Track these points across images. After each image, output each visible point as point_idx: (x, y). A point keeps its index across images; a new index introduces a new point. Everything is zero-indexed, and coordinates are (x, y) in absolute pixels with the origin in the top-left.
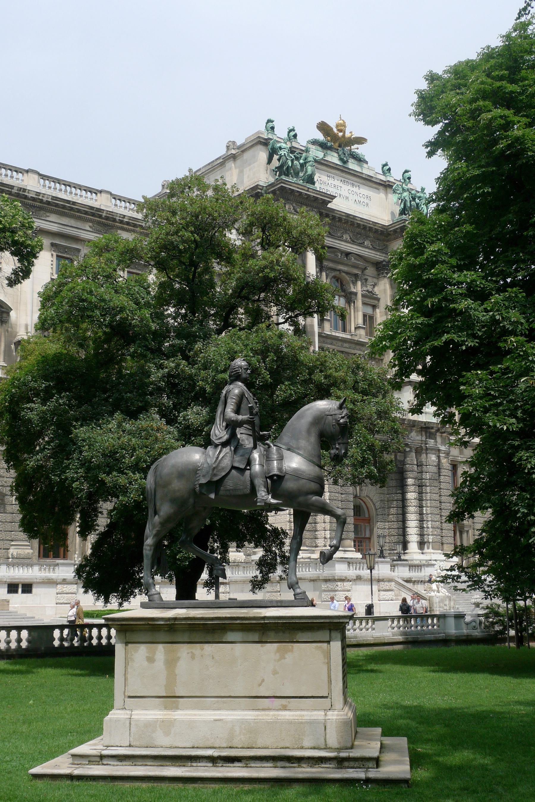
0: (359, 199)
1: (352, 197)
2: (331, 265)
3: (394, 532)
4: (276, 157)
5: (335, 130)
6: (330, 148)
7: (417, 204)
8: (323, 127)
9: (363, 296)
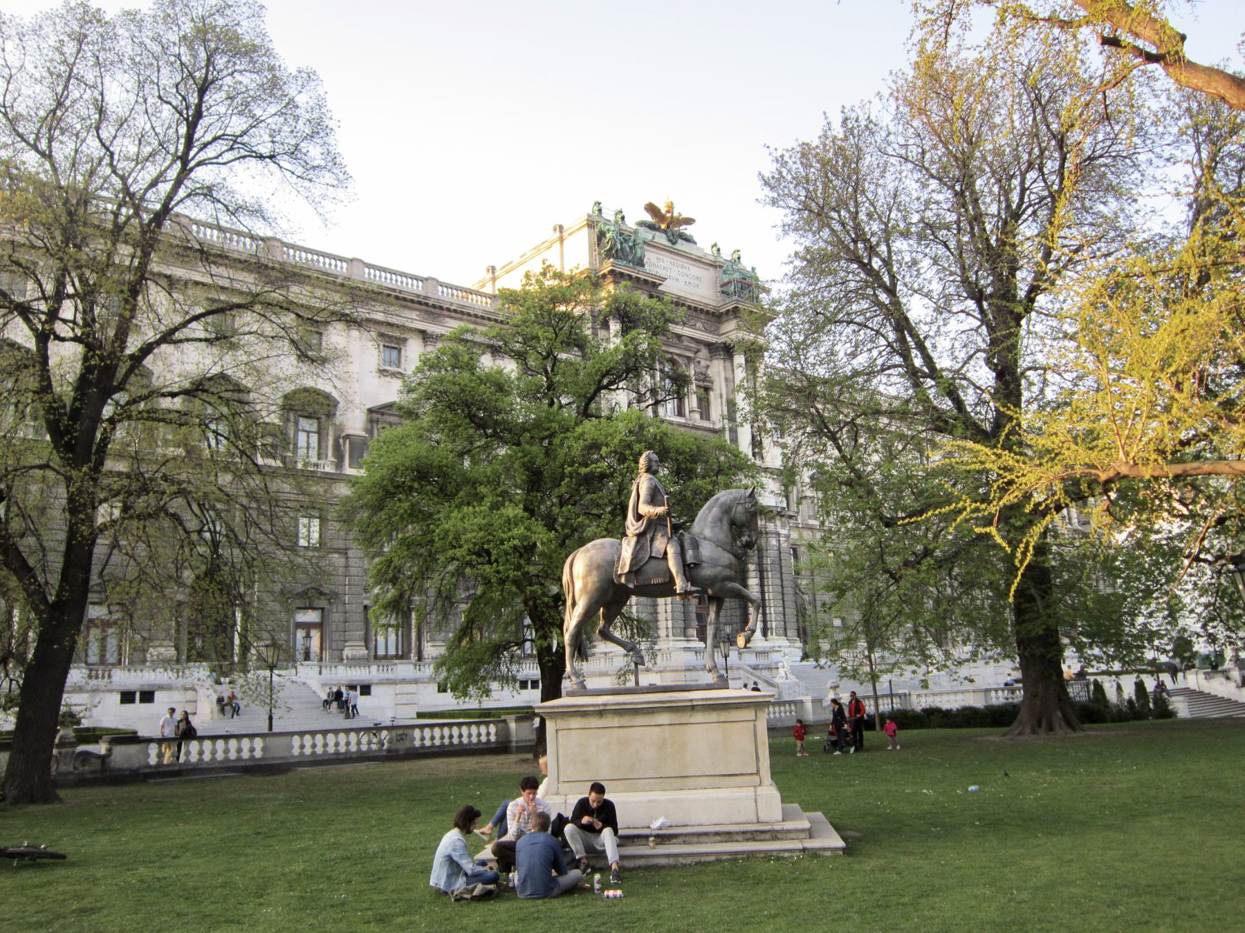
8: (651, 208)
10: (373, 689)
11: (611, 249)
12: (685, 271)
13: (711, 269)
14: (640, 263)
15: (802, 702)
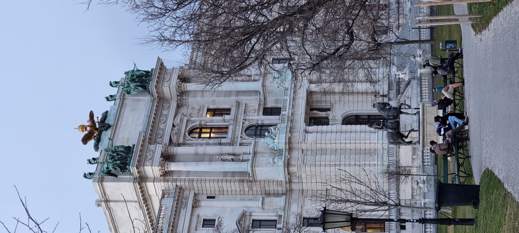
5: (86, 132)
7: (137, 77)
8: (85, 140)
11: (120, 167)
13: (125, 102)
15: (420, 74)
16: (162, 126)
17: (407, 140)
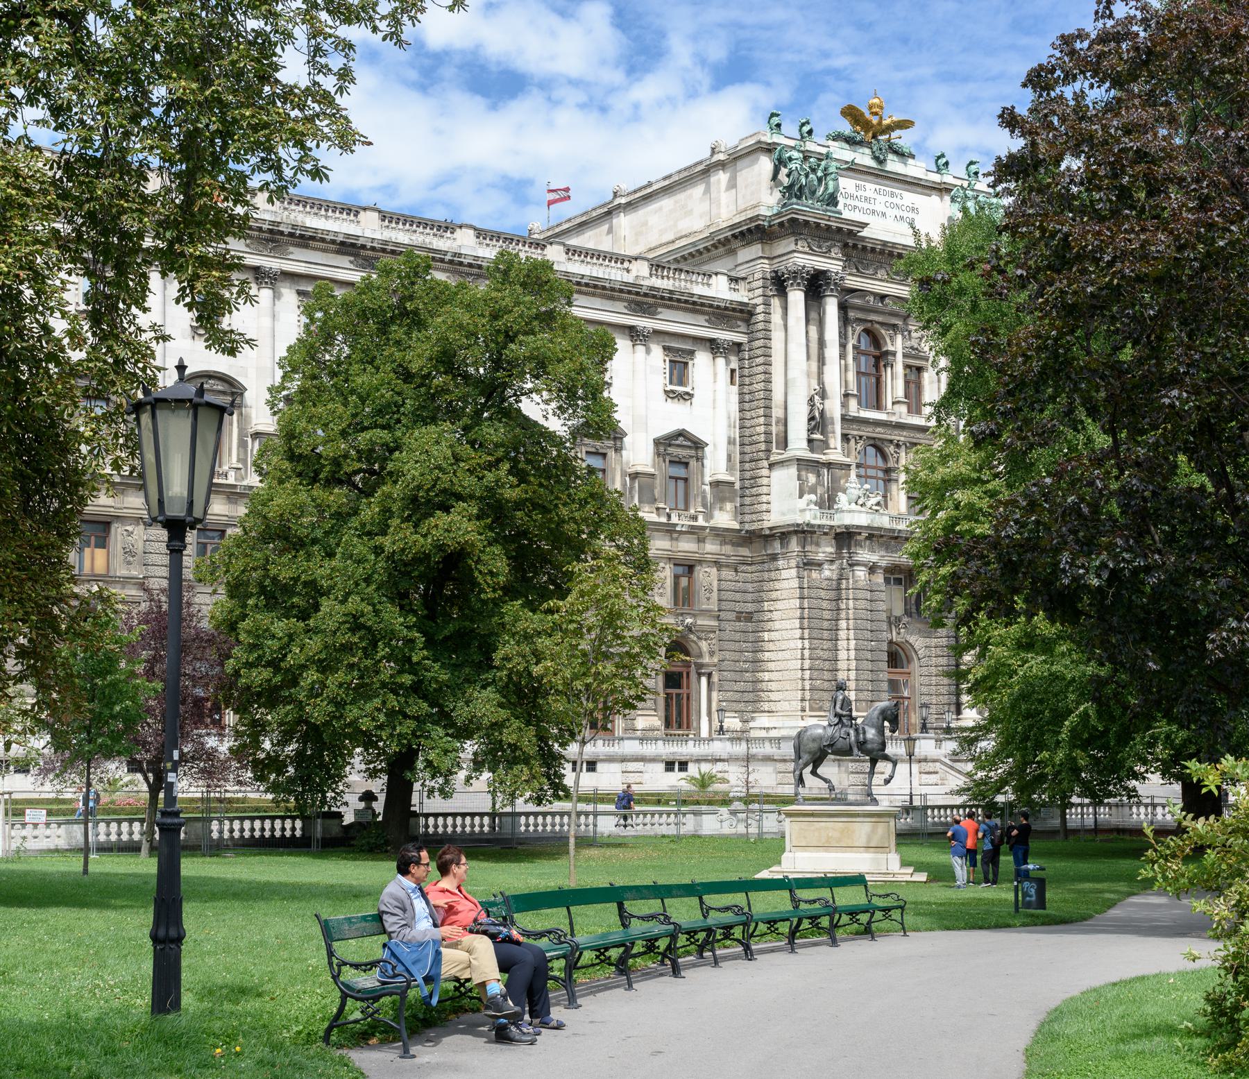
0: (902, 214)
1: (891, 213)
2: (860, 315)
3: (944, 690)
4: (784, 171)
6: (860, 143)
9: (905, 356)
10: (599, 766)
12: (895, 200)
14: (832, 200)
16: (881, 274)
17: (807, 771)
